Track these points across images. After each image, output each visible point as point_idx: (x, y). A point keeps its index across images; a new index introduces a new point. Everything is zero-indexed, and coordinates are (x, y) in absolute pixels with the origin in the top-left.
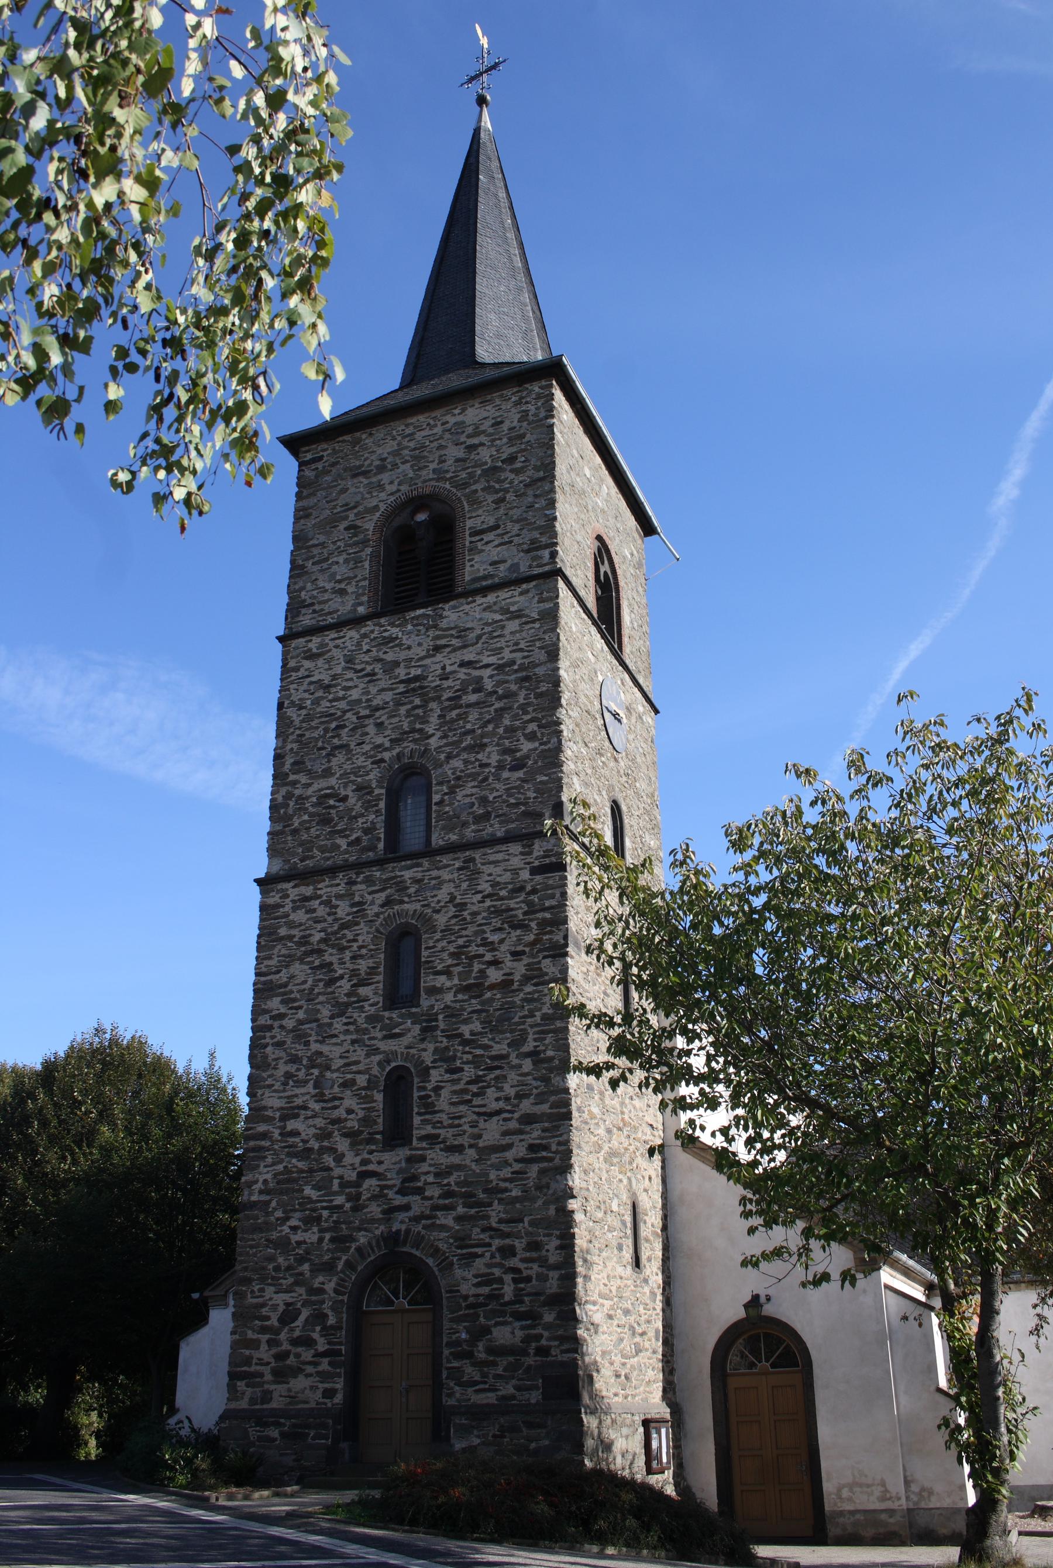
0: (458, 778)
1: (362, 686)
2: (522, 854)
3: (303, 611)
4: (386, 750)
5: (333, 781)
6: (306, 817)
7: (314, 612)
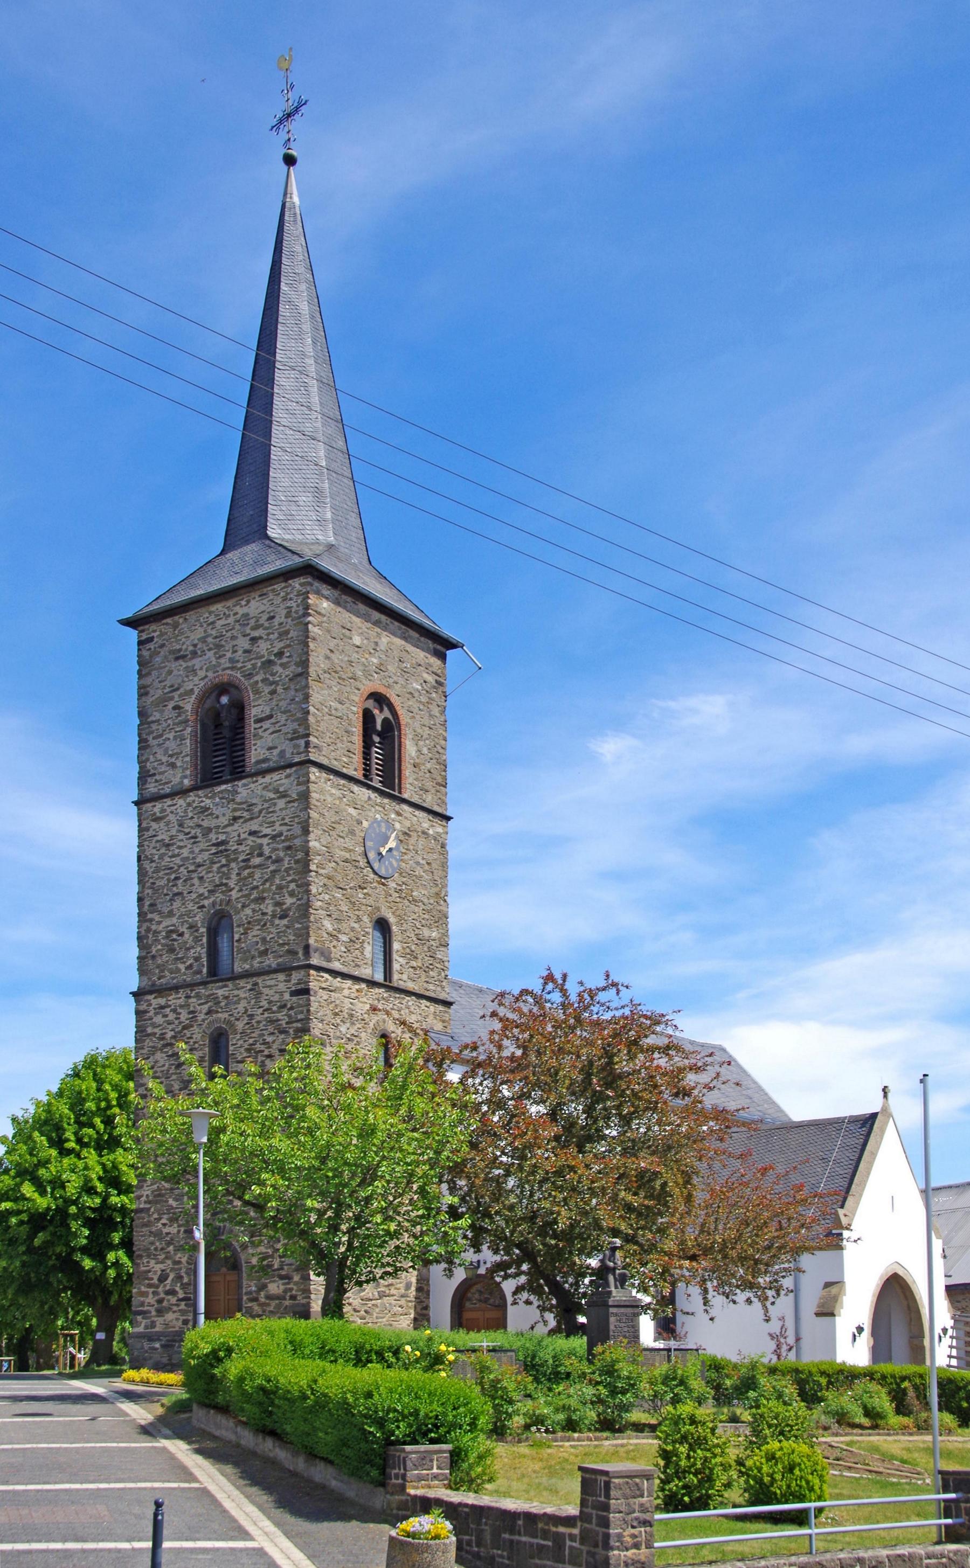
0: (249, 923)
1: (189, 846)
2: (285, 981)
3: (149, 779)
4: (206, 898)
5: (174, 920)
6: (159, 947)
7: (156, 781)
